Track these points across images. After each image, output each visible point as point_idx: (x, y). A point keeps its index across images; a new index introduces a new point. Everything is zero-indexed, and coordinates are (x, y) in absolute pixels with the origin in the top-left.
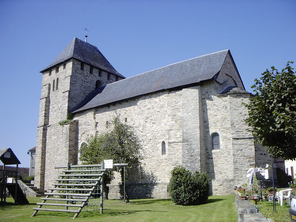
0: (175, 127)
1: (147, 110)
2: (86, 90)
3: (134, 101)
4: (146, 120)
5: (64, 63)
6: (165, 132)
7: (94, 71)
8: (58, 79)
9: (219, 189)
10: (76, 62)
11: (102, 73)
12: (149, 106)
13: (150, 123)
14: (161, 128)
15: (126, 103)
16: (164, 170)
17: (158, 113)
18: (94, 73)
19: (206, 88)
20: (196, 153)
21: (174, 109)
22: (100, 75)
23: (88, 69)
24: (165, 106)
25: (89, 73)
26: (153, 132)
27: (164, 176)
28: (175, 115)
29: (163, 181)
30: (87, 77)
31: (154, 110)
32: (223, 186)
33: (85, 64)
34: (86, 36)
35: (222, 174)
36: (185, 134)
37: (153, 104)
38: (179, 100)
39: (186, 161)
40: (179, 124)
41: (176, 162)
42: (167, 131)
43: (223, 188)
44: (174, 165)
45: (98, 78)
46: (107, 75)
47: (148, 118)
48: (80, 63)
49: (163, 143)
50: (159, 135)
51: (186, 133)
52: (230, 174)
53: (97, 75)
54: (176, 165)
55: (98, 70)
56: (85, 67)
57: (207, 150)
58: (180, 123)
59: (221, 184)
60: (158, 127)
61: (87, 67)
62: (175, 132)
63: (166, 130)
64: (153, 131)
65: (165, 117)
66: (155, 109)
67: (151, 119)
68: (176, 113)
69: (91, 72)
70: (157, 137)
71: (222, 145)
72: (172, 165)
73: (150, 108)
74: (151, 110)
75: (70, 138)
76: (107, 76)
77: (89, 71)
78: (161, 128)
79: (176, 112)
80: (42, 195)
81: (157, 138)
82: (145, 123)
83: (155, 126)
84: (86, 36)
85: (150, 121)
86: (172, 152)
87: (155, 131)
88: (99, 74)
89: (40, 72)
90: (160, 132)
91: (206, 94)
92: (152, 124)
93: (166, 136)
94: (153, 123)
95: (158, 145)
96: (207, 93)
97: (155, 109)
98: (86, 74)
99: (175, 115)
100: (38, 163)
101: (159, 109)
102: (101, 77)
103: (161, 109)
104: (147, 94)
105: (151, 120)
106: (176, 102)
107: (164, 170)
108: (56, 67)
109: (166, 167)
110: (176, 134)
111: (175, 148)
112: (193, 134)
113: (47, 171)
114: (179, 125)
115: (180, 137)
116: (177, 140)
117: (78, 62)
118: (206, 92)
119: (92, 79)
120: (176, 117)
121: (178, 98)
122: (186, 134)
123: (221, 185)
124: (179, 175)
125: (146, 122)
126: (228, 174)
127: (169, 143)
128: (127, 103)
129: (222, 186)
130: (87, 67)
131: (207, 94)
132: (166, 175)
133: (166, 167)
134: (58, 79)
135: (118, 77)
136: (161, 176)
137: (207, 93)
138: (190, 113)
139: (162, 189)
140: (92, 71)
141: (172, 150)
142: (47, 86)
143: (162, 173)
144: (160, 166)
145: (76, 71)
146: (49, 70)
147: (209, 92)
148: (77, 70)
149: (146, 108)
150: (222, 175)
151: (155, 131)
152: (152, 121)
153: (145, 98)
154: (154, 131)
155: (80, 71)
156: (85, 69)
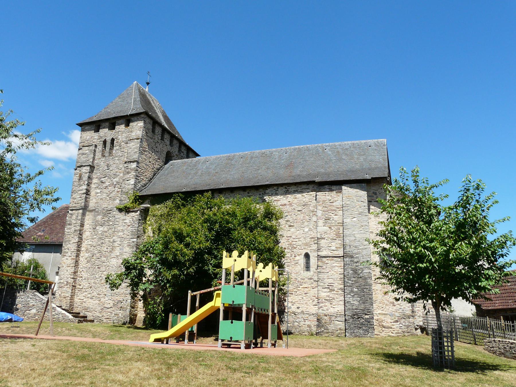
0: (328, 235)
5: (128, 120)
6: (309, 240)
8: (113, 140)
9: (393, 327)
16: (306, 294)
17: (299, 212)
18: (165, 140)
21: (328, 210)
22: (171, 144)
26: (289, 238)
29: (304, 309)
30: (158, 145)
31: (293, 207)
34: (148, 84)
35: (395, 306)
38: (336, 199)
40: (334, 231)
49: (307, 256)
50: (300, 243)
52: (407, 308)
54: (329, 288)
57: (73, 286)
60: (298, 232)
66: (293, 207)
67: (286, 219)
70: (295, 246)
79: (331, 214)
81: (295, 248)
83: (293, 230)
84: (148, 84)
85: (285, 222)
87: (293, 237)
89: (77, 124)
90: (301, 239)
91: (373, 195)
95: (297, 258)
96: (376, 194)
97: (293, 207)
104: (282, 185)
105: (287, 221)
107: (306, 294)
110: (330, 245)
112: (360, 248)
113: (84, 281)
114: (335, 233)
116: (331, 254)
123: (397, 321)
126: (404, 306)
127: (319, 257)
128: (245, 193)
129: (398, 323)
131: (375, 196)
134: (113, 140)
135: (190, 153)
137: (376, 194)
138: (355, 219)
139: (305, 321)
141: (324, 267)
142: (93, 148)
143: (303, 298)
146: (96, 125)
147: (377, 193)
150: (395, 308)
151: (293, 237)
152: (289, 223)
153: (278, 188)
156: (156, 131)
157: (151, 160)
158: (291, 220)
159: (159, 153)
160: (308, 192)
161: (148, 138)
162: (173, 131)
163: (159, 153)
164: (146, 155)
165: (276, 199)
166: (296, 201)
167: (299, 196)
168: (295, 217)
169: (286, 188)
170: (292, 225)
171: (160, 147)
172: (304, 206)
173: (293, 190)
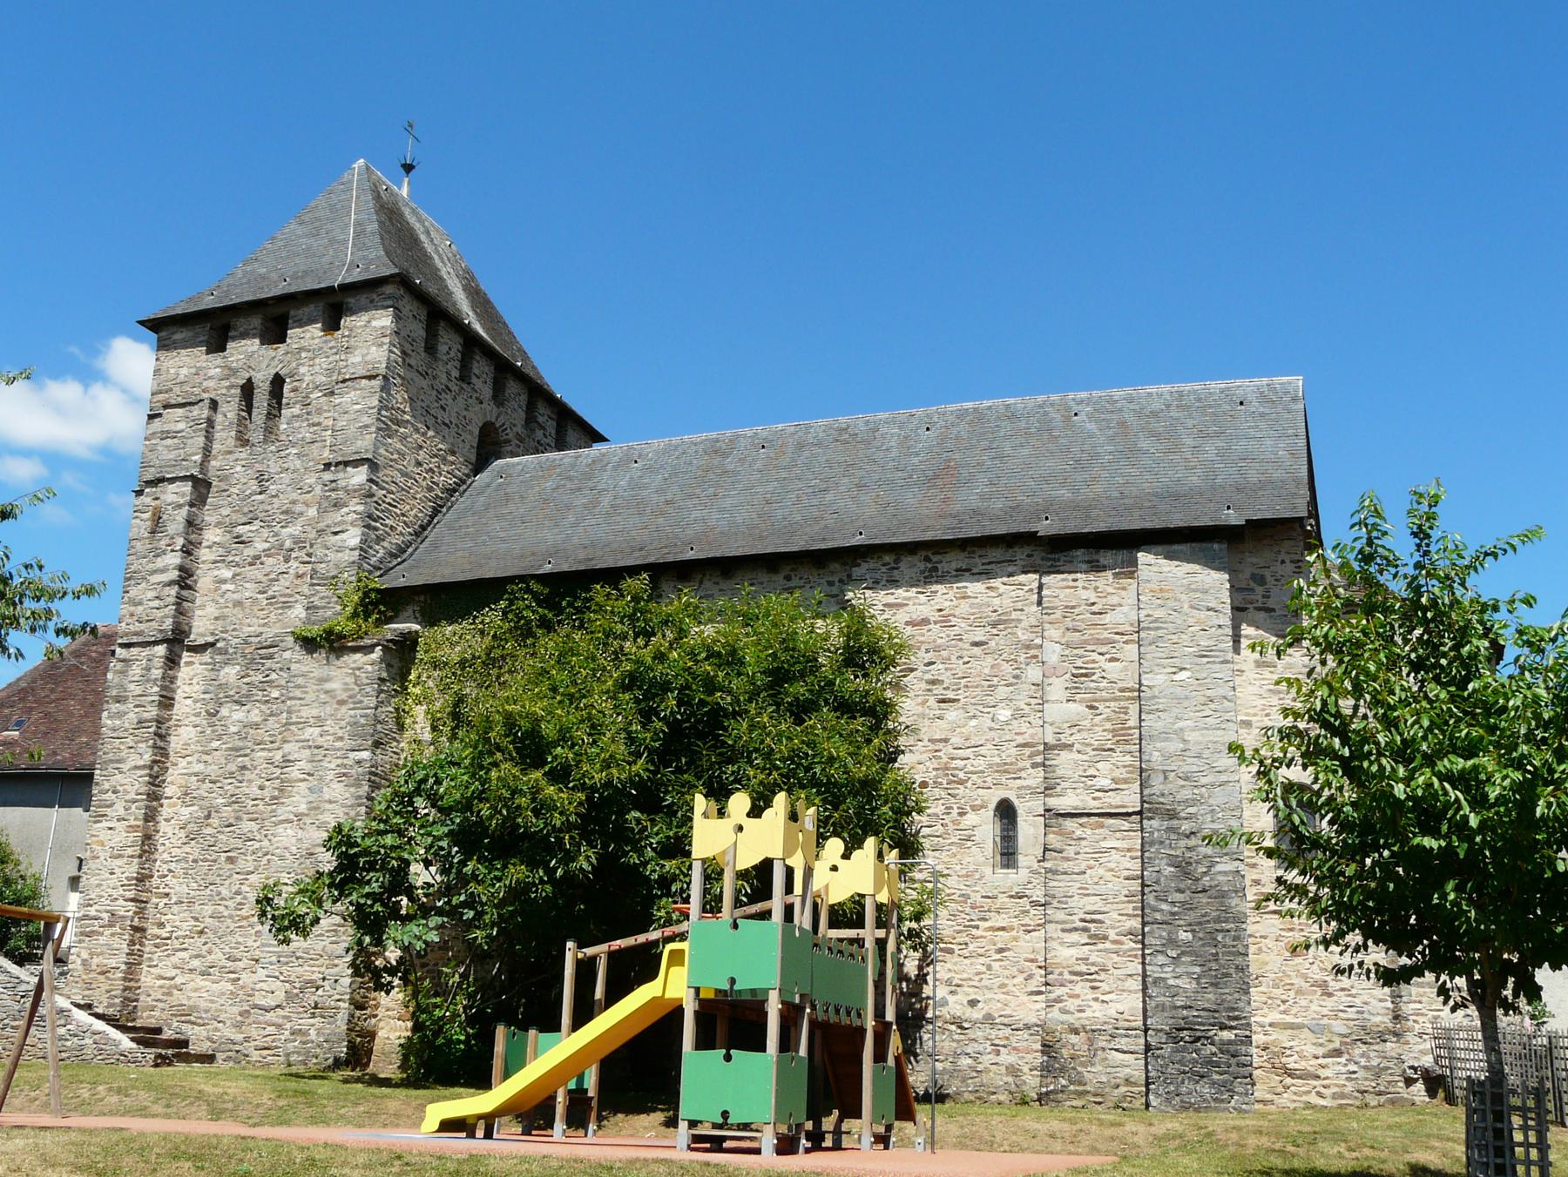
3: (815, 572)
5: (333, 305)
6: (1013, 751)
8: (278, 382)
9: (1323, 1073)
13: (920, 699)
14: (991, 729)
15: (763, 577)
17: (977, 650)
18: (474, 380)
19: (1254, 560)
20: (1221, 878)
21: (1086, 642)
22: (498, 396)
23: (452, 354)
24: (1019, 621)
26: (940, 746)
27: (1003, 985)
28: (1086, 675)
29: (995, 1009)
32: (1346, 1056)
34: (408, 168)
36: (1161, 778)
37: (947, 604)
39: (1168, 918)
40: (1108, 719)
41: (1088, 917)
42: (1027, 751)
43: (1344, 1070)
44: (1076, 929)
47: (912, 670)
49: (1006, 812)
50: (980, 764)
51: (1164, 772)
52: (1374, 1002)
58: (1114, 716)
59: (1337, 1045)
60: (973, 723)
62: (1085, 757)
63: (1025, 745)
64: (940, 741)
65: (1016, 677)
67: (928, 677)
68: (1094, 662)
69: (465, 376)
71: (167, 820)
72: (1063, 930)
75: (379, 727)
77: (458, 364)
78: (991, 729)
79: (1095, 656)
80: (177, 1056)
81: (961, 782)
83: (952, 714)
84: (408, 168)
85: (924, 686)
86: (1068, 859)
87: (955, 740)
88: (495, 390)
89: (141, 323)
90: (983, 750)
92: (932, 701)
93: (1023, 774)
94: (943, 701)
95: (971, 819)
96: (1261, 581)
99: (1086, 675)
100: (120, 856)
103: (995, 631)
105: (933, 682)
106: (1095, 609)
108: (273, 317)
109: (1016, 939)
111: (1083, 843)
114: (1108, 726)
115: (1114, 786)
116: (1096, 804)
118: (1253, 577)
120: (1093, 685)
121: (1110, 590)
122: (1166, 778)
123: (1337, 1053)
124: (412, 978)
126: (1365, 998)
127: (1053, 816)
128: (775, 578)
131: (1260, 590)
132: (1015, 981)
133: (1016, 939)
134: (278, 382)
136: (984, 983)
137: (1261, 581)
138: (1183, 675)
139: (998, 1053)
141: (1070, 852)
142: (202, 412)
144: (977, 927)
146: (213, 326)
147: (1269, 578)
148: (408, 348)
150: (1330, 1003)
151: (955, 740)
152: (938, 690)
153: (897, 561)
154: (946, 741)
156: (443, 349)
158: (947, 678)
159: (454, 429)
163: (454, 429)
164: (404, 438)
166: (964, 607)
167: (975, 588)
169: (927, 559)
170: (951, 695)
172: (994, 626)
173: (954, 565)
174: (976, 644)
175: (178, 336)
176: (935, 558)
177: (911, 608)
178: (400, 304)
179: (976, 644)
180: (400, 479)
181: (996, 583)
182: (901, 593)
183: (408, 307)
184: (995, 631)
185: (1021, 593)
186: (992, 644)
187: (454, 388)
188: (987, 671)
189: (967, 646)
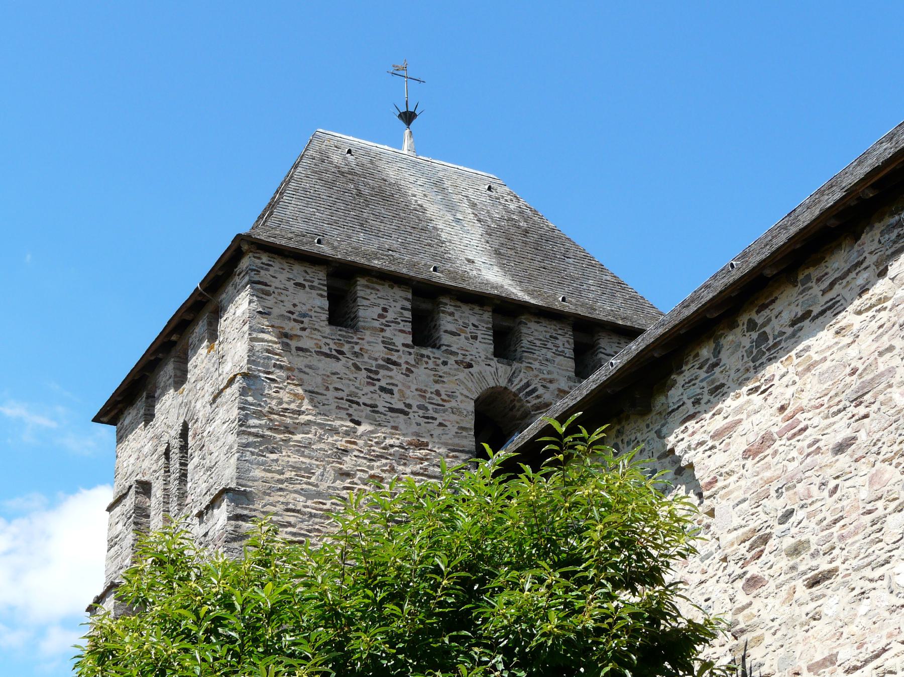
1: (749, 463)
2: (393, 470)
4: (753, 569)
7: (447, 322)
10: (280, 275)
11: (524, 330)
12: (756, 418)
17: (844, 460)
18: (446, 339)
22: (505, 346)
23: (390, 316)
25: (409, 340)
33: (362, 281)
45: (493, 374)
46: (565, 341)
47: (765, 539)
48: (319, 277)
53: (483, 348)
55: (487, 316)
56: (360, 302)
61: (382, 303)
69: (424, 332)
73: (767, 440)
74: (787, 457)
76: (570, 353)
77: (408, 327)
82: (742, 599)
83: (834, 601)
84: (408, 117)
94: (814, 583)
98: (379, 351)
101: (841, 421)
102: (516, 365)
103: (862, 410)
105: (795, 551)
117: (298, 272)
119: (437, 387)
125: (754, 583)
130: (382, 303)
140: (436, 327)
145: (286, 335)
148: (291, 327)
149: (738, 444)
152: (805, 563)
153: (717, 352)
155: (322, 334)
157: (348, 463)
158: (813, 536)
159: (415, 416)
160: (864, 290)
161: (300, 362)
162: (454, 279)
163: (415, 416)
164: (303, 448)
165: (719, 423)
166: (813, 386)
167: (820, 342)
168: (828, 507)
169: (752, 326)
170: (824, 565)
171: (416, 379)
172: (857, 401)
173: (787, 317)
174: (840, 448)
175: (127, 422)
176: (760, 319)
177: (745, 425)
178: (264, 276)
179: (840, 448)
180: (300, 502)
181: (848, 317)
182: (729, 404)
183: (283, 276)
184: (862, 410)
185: (884, 315)
186: (862, 436)
187: (402, 357)
188: (864, 494)
189: (828, 458)
